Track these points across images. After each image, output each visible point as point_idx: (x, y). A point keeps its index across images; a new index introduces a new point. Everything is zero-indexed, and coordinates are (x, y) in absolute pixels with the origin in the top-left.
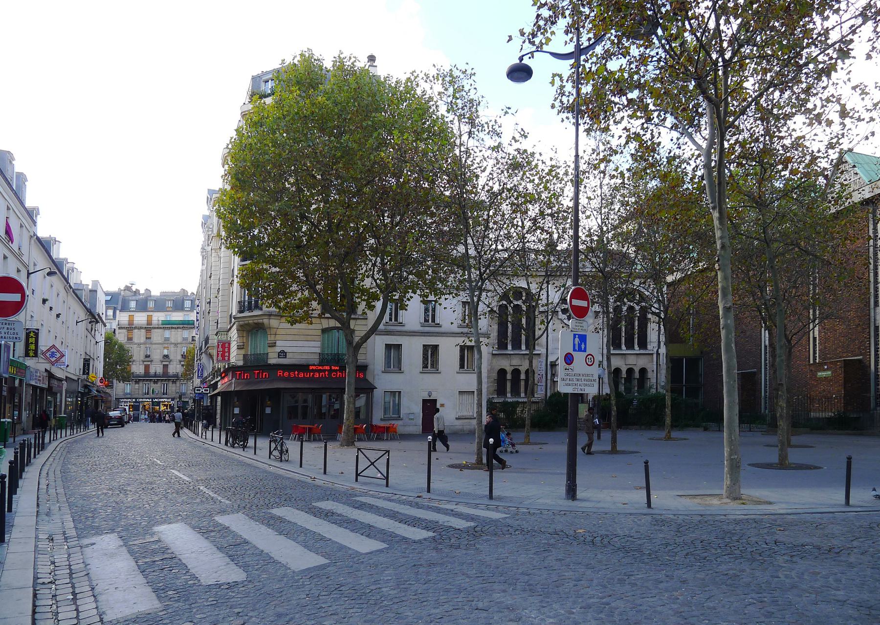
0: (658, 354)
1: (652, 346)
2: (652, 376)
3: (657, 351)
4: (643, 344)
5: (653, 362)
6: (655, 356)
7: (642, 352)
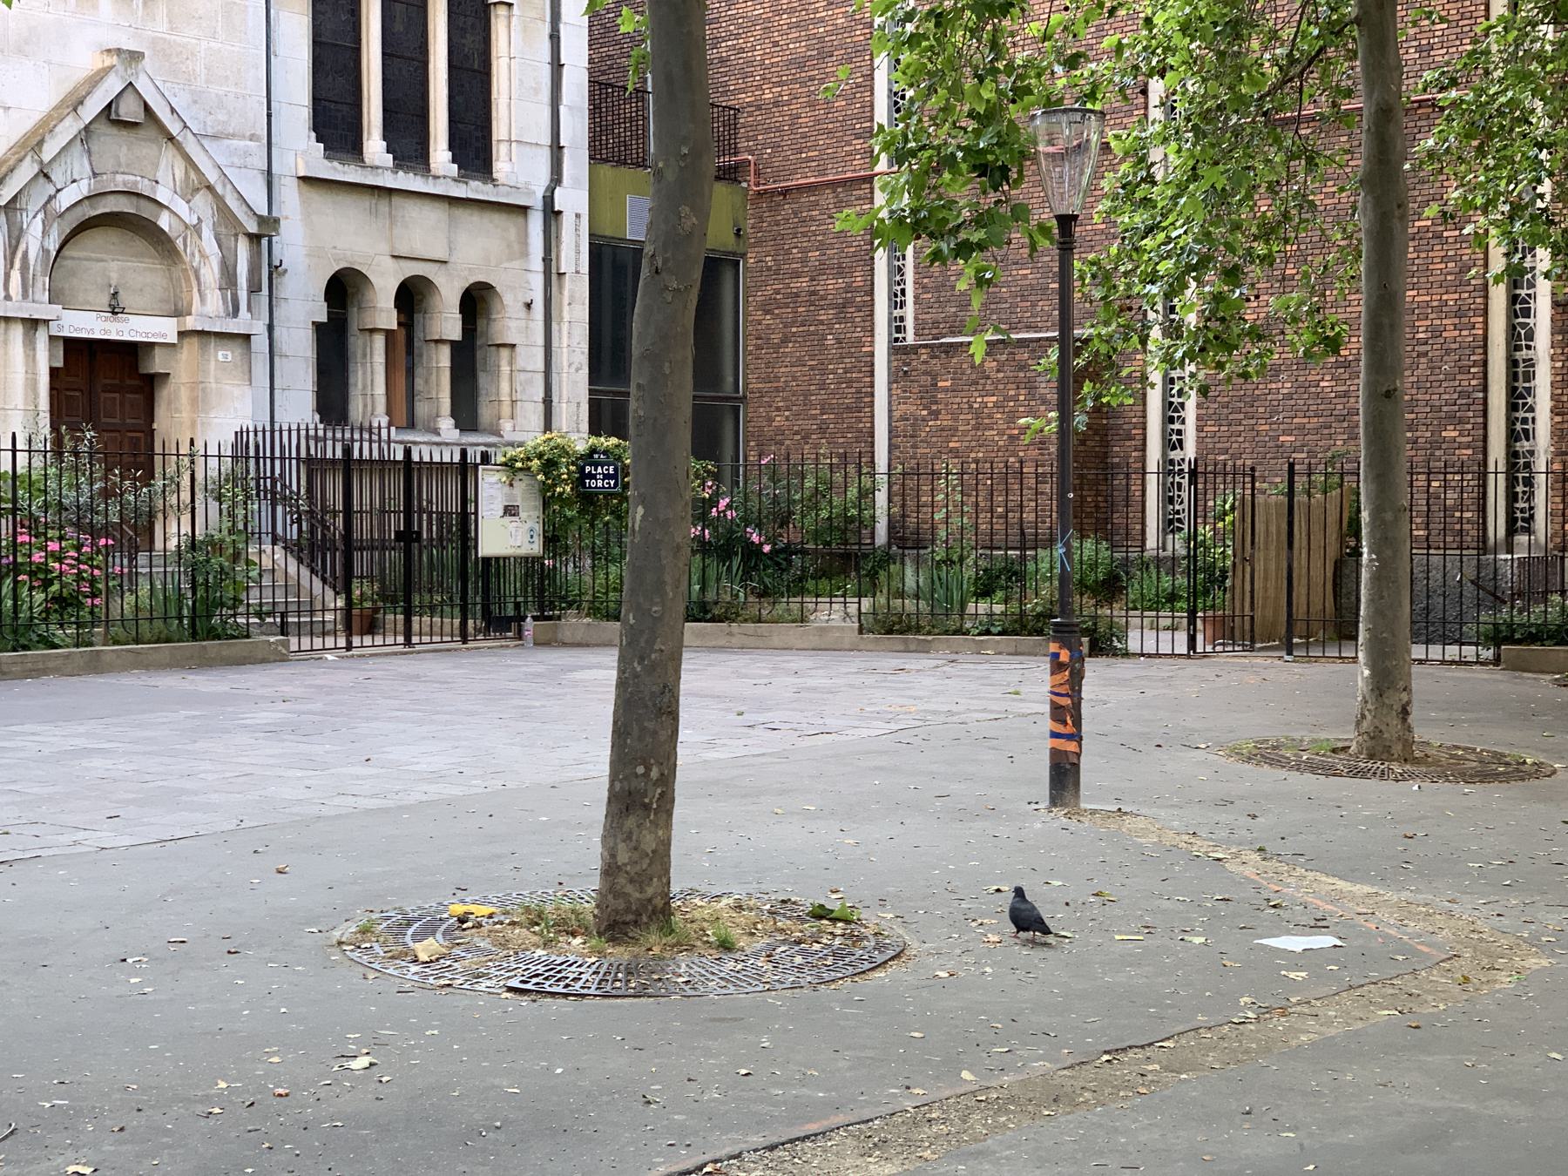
0: (552, 214)
1: (518, 166)
2: (515, 324)
3: (549, 200)
4: (474, 149)
5: (525, 254)
6: (536, 222)
7: (475, 189)
